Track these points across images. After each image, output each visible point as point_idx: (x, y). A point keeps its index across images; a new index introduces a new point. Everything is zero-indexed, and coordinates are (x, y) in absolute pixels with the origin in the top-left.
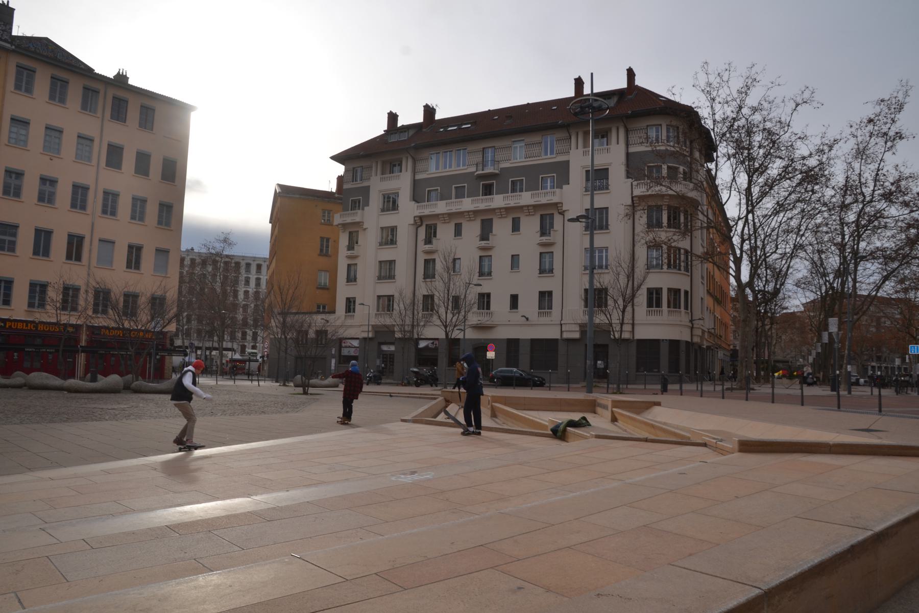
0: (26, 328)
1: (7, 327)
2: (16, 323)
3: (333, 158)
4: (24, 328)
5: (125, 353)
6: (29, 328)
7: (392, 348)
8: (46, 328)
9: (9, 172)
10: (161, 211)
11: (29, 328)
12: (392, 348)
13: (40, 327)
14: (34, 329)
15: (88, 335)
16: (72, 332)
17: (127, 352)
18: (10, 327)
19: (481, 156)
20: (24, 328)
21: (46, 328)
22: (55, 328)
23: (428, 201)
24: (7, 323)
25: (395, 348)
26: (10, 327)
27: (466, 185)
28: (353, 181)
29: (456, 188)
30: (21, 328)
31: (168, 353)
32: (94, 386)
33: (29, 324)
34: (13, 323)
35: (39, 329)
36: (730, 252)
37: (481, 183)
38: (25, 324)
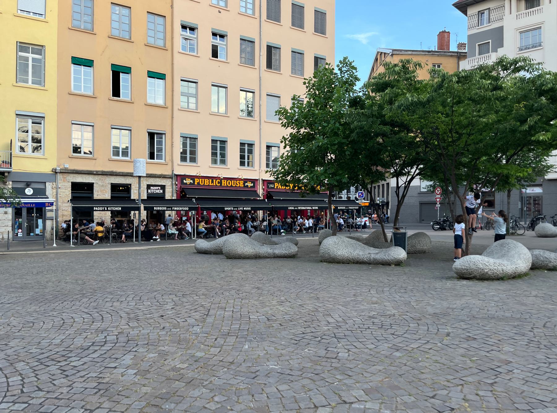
0: (212, 184)
1: (196, 183)
2: (203, 180)
3: (453, 5)
4: (210, 184)
5: (310, 208)
6: (214, 184)
7: (538, 190)
8: (229, 182)
9: (23, 47)
10: (293, 59)
11: (214, 184)
12: (538, 190)
13: (224, 183)
14: (219, 185)
15: (264, 189)
16: (251, 187)
17: (312, 207)
18: (198, 183)
19: (477, 19)
20: (210, 184)
21: (229, 182)
22: (236, 184)
23: (479, 54)
24: (196, 179)
25: (543, 190)
26: (198, 183)
27: (490, 41)
28: (478, 26)
29: (479, 45)
30: (208, 184)
31: (234, 208)
32: (209, 247)
33: (214, 180)
34: (201, 180)
35: (223, 185)
36: (302, 131)
37: (477, 44)
38: (210, 180)
